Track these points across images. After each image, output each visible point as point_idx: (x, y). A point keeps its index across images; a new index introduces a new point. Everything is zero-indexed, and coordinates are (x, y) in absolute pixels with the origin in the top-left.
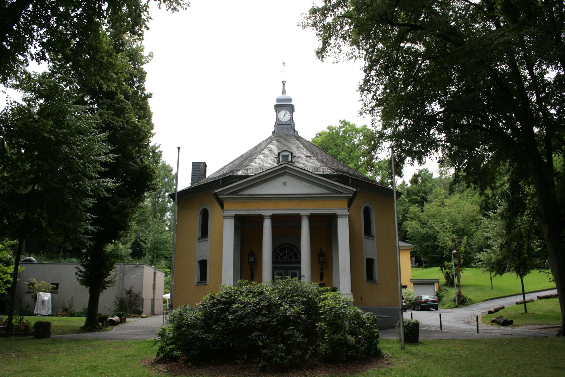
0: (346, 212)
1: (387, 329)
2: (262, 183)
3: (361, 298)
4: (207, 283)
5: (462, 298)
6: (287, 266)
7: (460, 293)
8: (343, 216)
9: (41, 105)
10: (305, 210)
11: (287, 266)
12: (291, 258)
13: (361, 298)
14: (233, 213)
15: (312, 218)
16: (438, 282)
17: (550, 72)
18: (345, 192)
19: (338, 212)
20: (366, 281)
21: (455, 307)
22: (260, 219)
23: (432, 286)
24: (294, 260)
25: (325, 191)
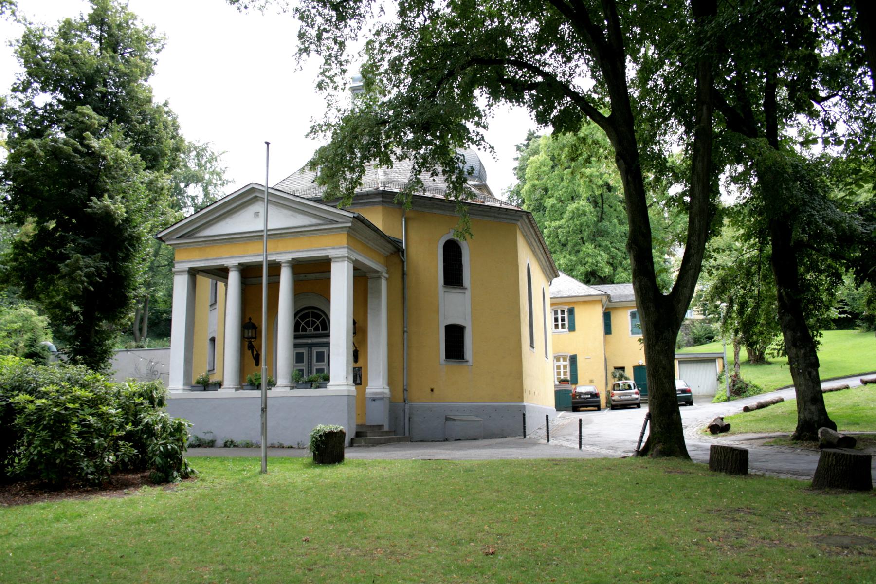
0: (344, 252)
1: (475, 439)
2: (225, 218)
3: (432, 390)
4: (470, 363)
5: (739, 385)
6: (309, 341)
7: (736, 375)
8: (340, 259)
9: (729, 76)
10: (284, 254)
11: (309, 341)
12: (317, 329)
13: (432, 390)
14: (186, 266)
15: (297, 266)
16: (722, 358)
17: (22, 14)
18: (340, 220)
19: (331, 253)
20: (444, 363)
21: (725, 401)
22: (275, 268)
23: (713, 364)
24: (321, 332)
25: (314, 221)
